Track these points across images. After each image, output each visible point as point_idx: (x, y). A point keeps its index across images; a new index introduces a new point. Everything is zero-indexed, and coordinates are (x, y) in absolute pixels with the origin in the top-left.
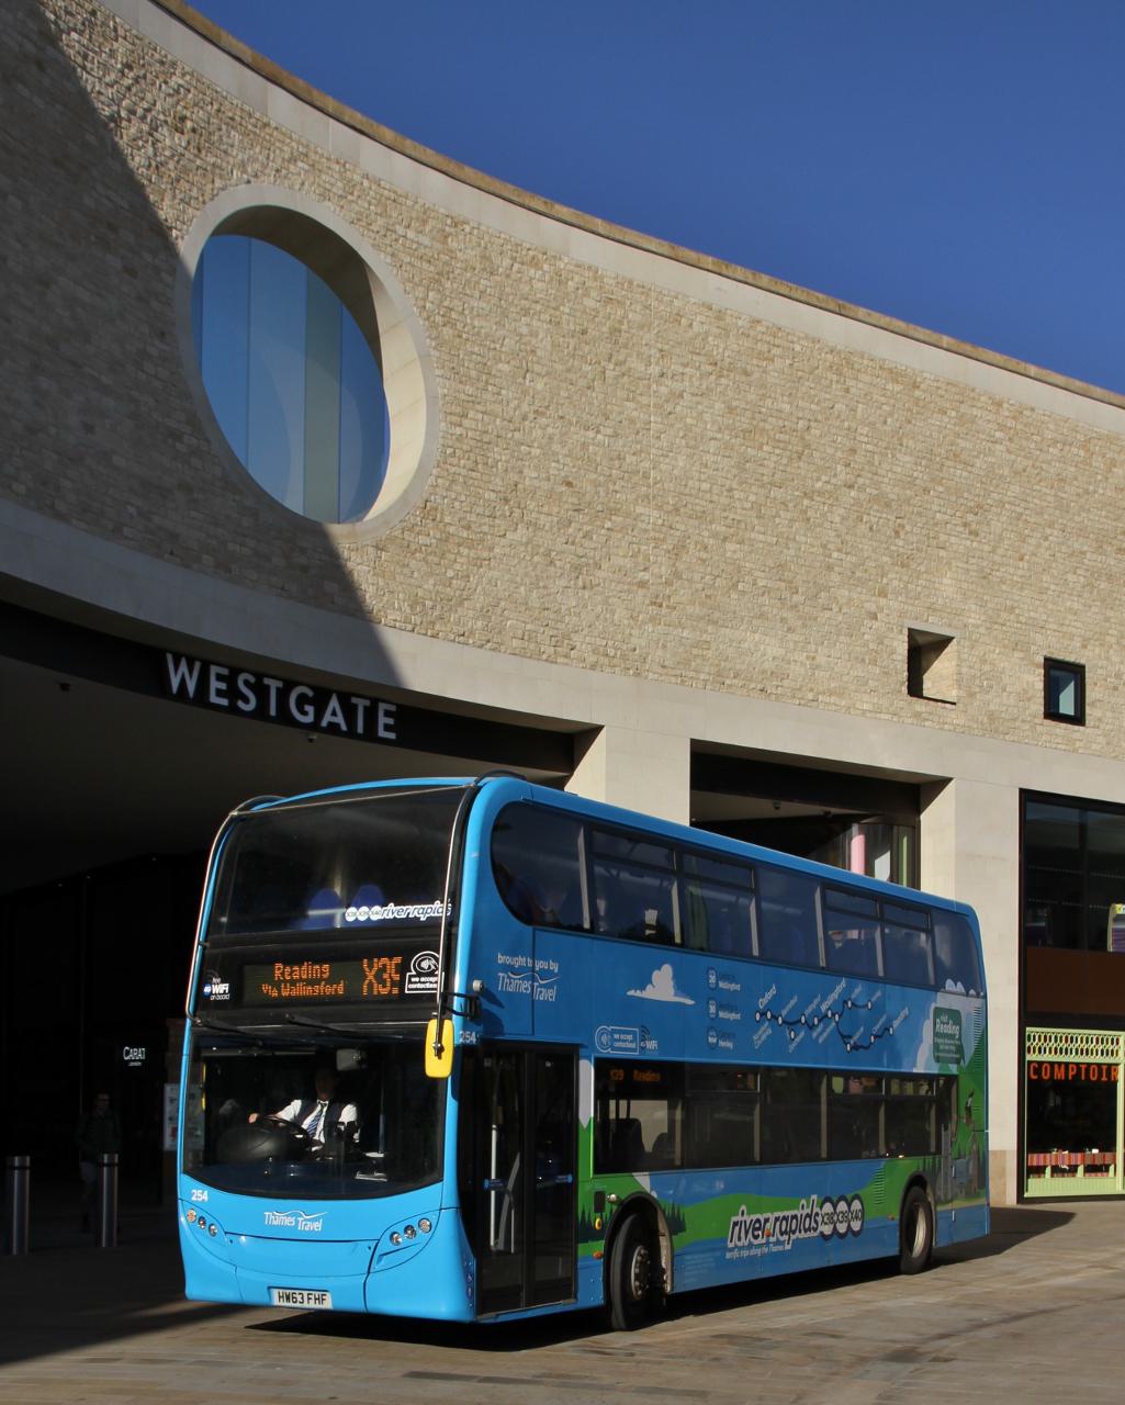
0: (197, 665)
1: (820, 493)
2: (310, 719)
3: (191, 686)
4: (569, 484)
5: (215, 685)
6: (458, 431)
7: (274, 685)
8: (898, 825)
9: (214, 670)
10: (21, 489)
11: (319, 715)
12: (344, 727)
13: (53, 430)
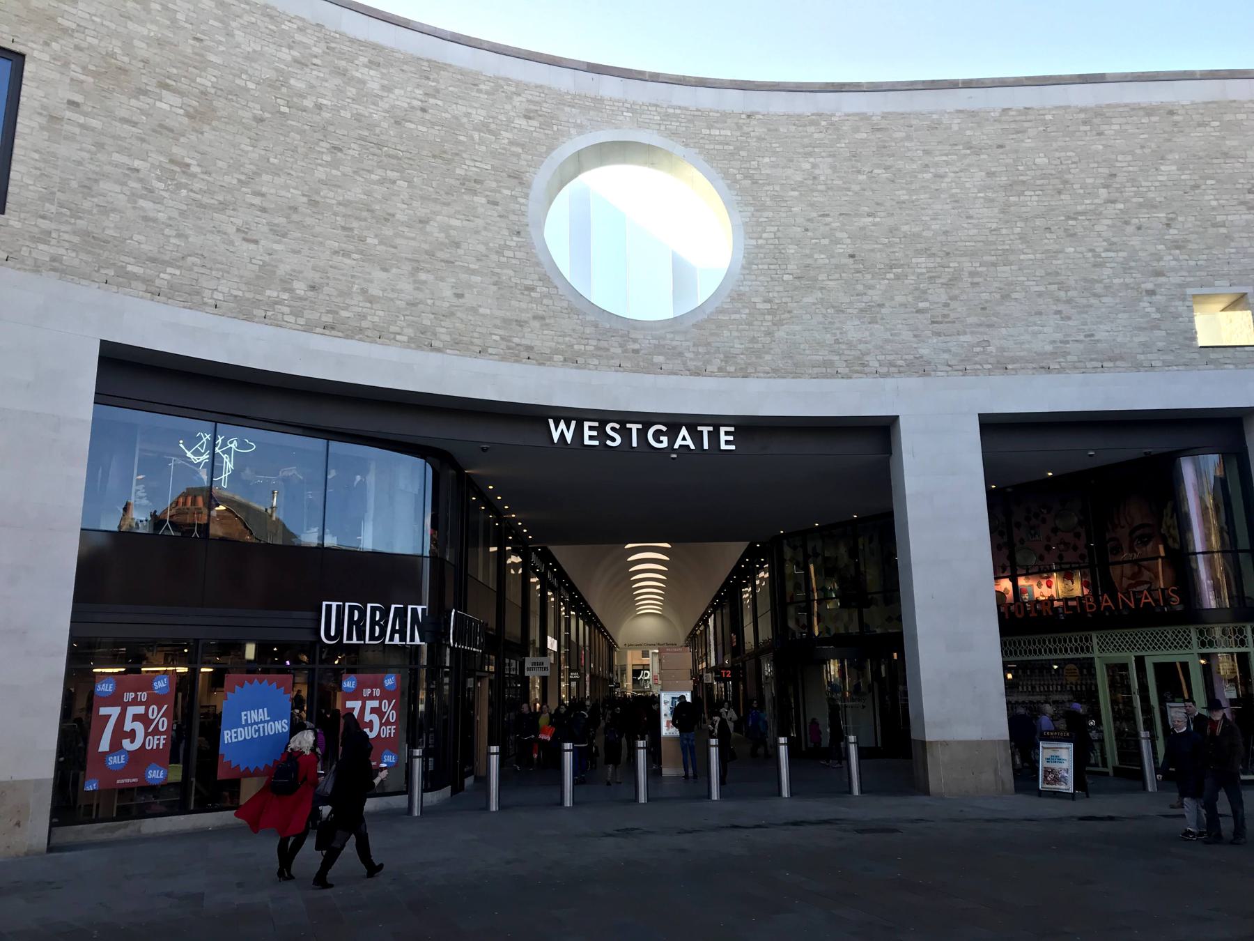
0: (573, 423)
1: (1083, 213)
2: (665, 444)
3: (569, 437)
4: (852, 256)
5: (587, 433)
6: (760, 242)
10: (405, 338)
11: (672, 441)
12: (692, 447)
13: (430, 302)
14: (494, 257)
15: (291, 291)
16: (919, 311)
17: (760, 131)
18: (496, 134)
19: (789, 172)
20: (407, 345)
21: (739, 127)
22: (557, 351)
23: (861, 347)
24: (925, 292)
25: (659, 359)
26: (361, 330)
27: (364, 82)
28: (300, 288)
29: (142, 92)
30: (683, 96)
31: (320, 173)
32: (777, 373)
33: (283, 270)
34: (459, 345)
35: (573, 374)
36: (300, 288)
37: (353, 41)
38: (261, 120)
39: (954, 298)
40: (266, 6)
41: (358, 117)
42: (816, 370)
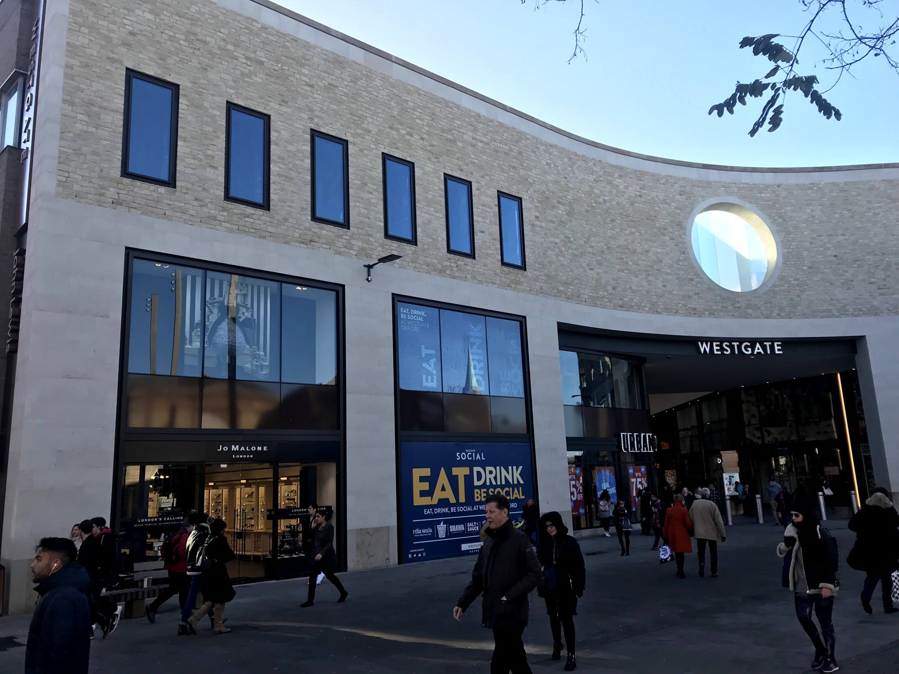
3: (708, 350)
4: (835, 256)
5: (715, 348)
7: (736, 344)
8: (692, 427)
9: (715, 344)
11: (753, 350)
14: (676, 266)
15: (607, 291)
16: (871, 283)
17: (784, 194)
18: (669, 204)
19: (801, 214)
20: (648, 312)
21: (774, 192)
22: (705, 310)
23: (844, 301)
24: (873, 273)
25: (750, 311)
26: (632, 306)
27: (618, 186)
28: (609, 288)
29: (554, 207)
30: (746, 177)
31: (609, 233)
32: (804, 316)
33: (603, 281)
34: (668, 310)
35: (712, 321)
36: (609, 288)
37: (612, 166)
38: (587, 211)
39: (889, 276)
40: (583, 156)
41: (618, 204)
42: (823, 314)
